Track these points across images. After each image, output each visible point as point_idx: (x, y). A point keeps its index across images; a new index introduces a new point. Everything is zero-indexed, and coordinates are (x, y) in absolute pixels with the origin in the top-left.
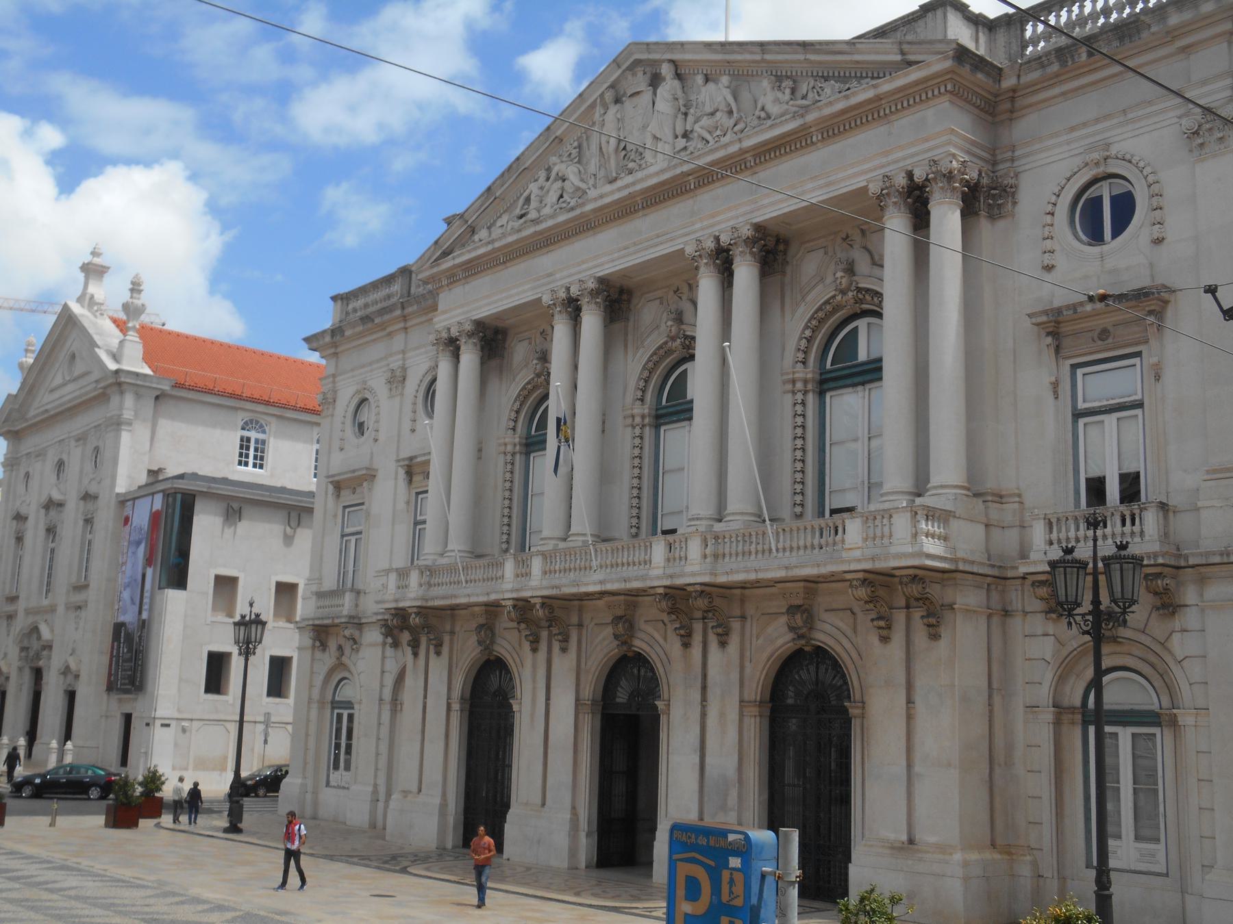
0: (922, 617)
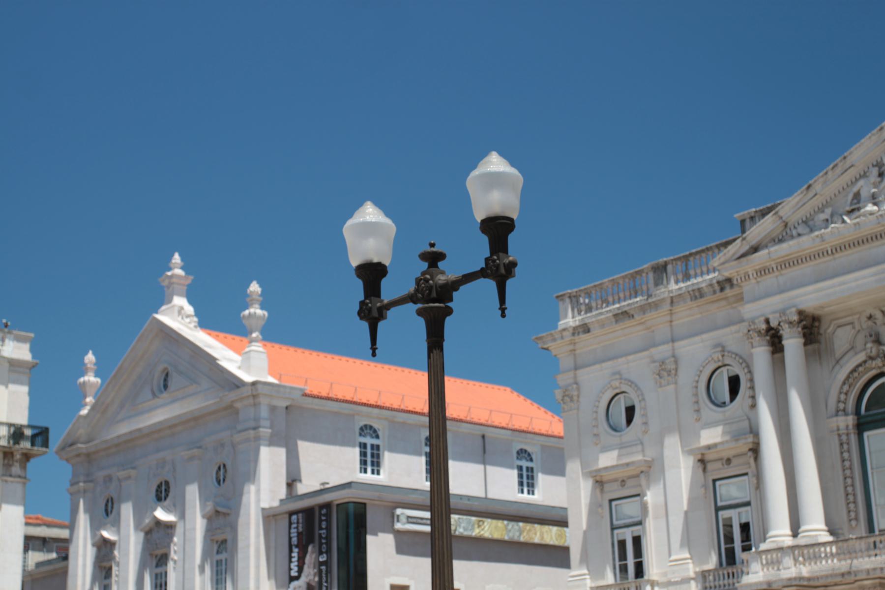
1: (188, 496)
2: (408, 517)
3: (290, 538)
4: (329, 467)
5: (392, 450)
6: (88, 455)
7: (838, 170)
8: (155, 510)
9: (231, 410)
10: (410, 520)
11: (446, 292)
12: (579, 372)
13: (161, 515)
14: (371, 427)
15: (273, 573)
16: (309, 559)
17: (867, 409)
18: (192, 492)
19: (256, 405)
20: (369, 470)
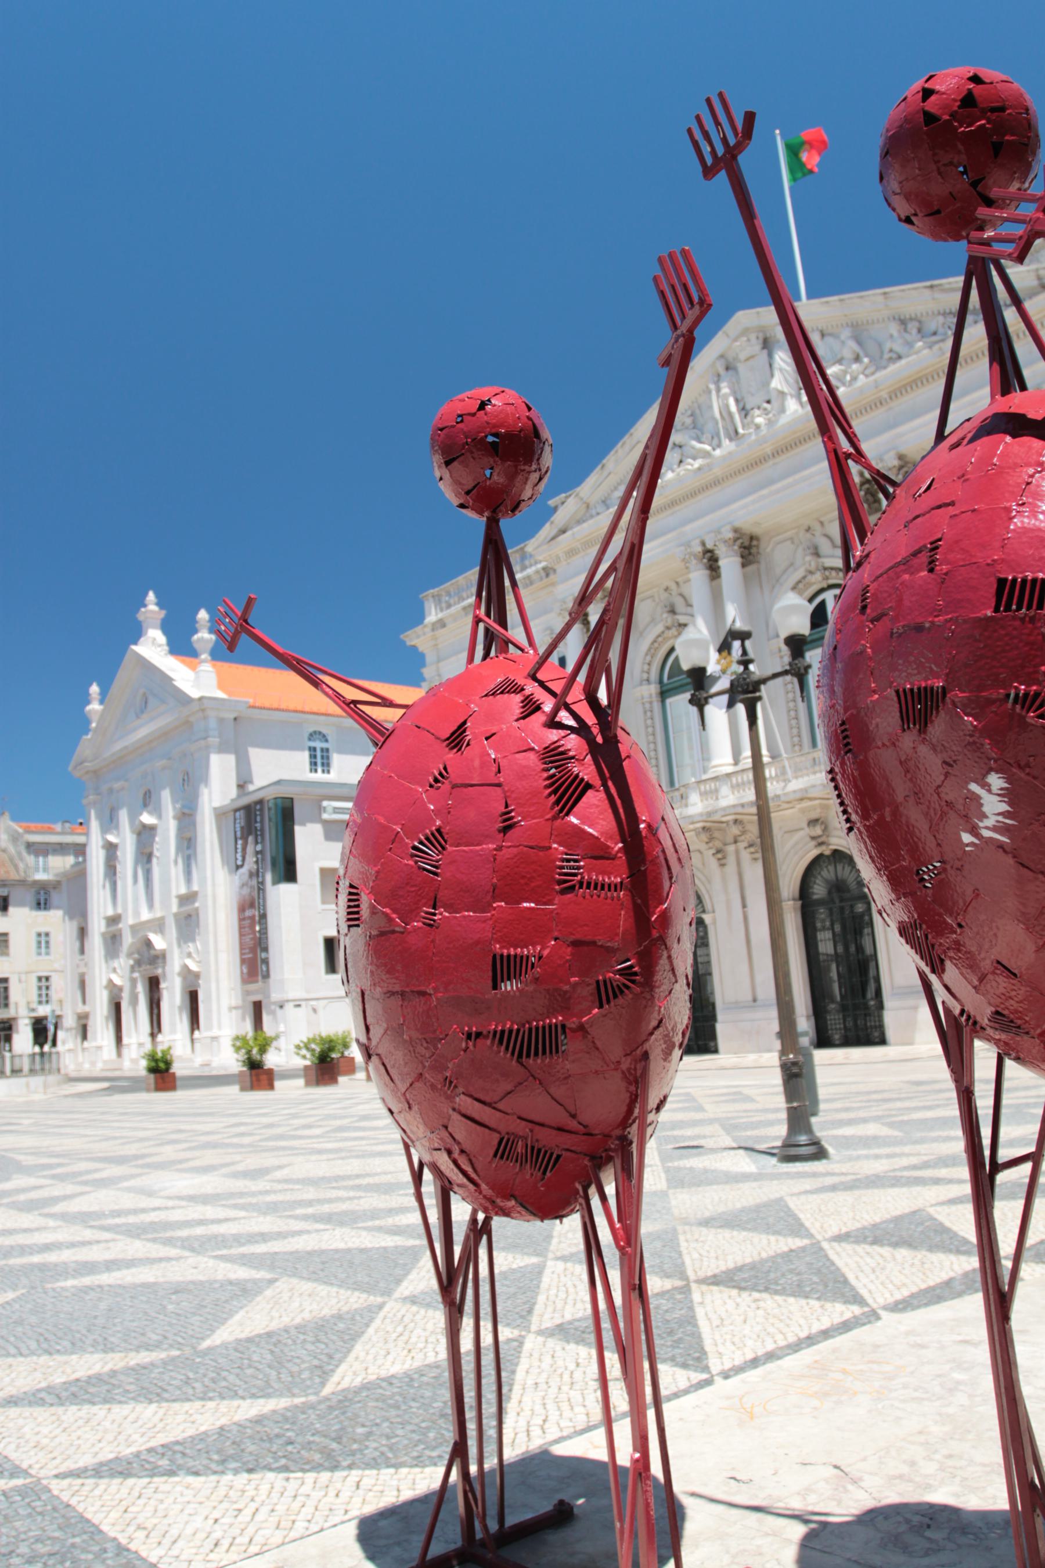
0: (714, 854)
1: (163, 802)
2: (335, 808)
3: (235, 832)
4: (277, 768)
5: (340, 751)
6: (95, 772)
7: (627, 447)
8: (141, 814)
9: (187, 724)
10: (336, 810)
11: (756, 685)
12: (441, 664)
13: (147, 819)
14: (320, 733)
15: (225, 861)
16: (250, 849)
17: (669, 678)
18: (166, 795)
19: (205, 718)
20: (320, 770)
